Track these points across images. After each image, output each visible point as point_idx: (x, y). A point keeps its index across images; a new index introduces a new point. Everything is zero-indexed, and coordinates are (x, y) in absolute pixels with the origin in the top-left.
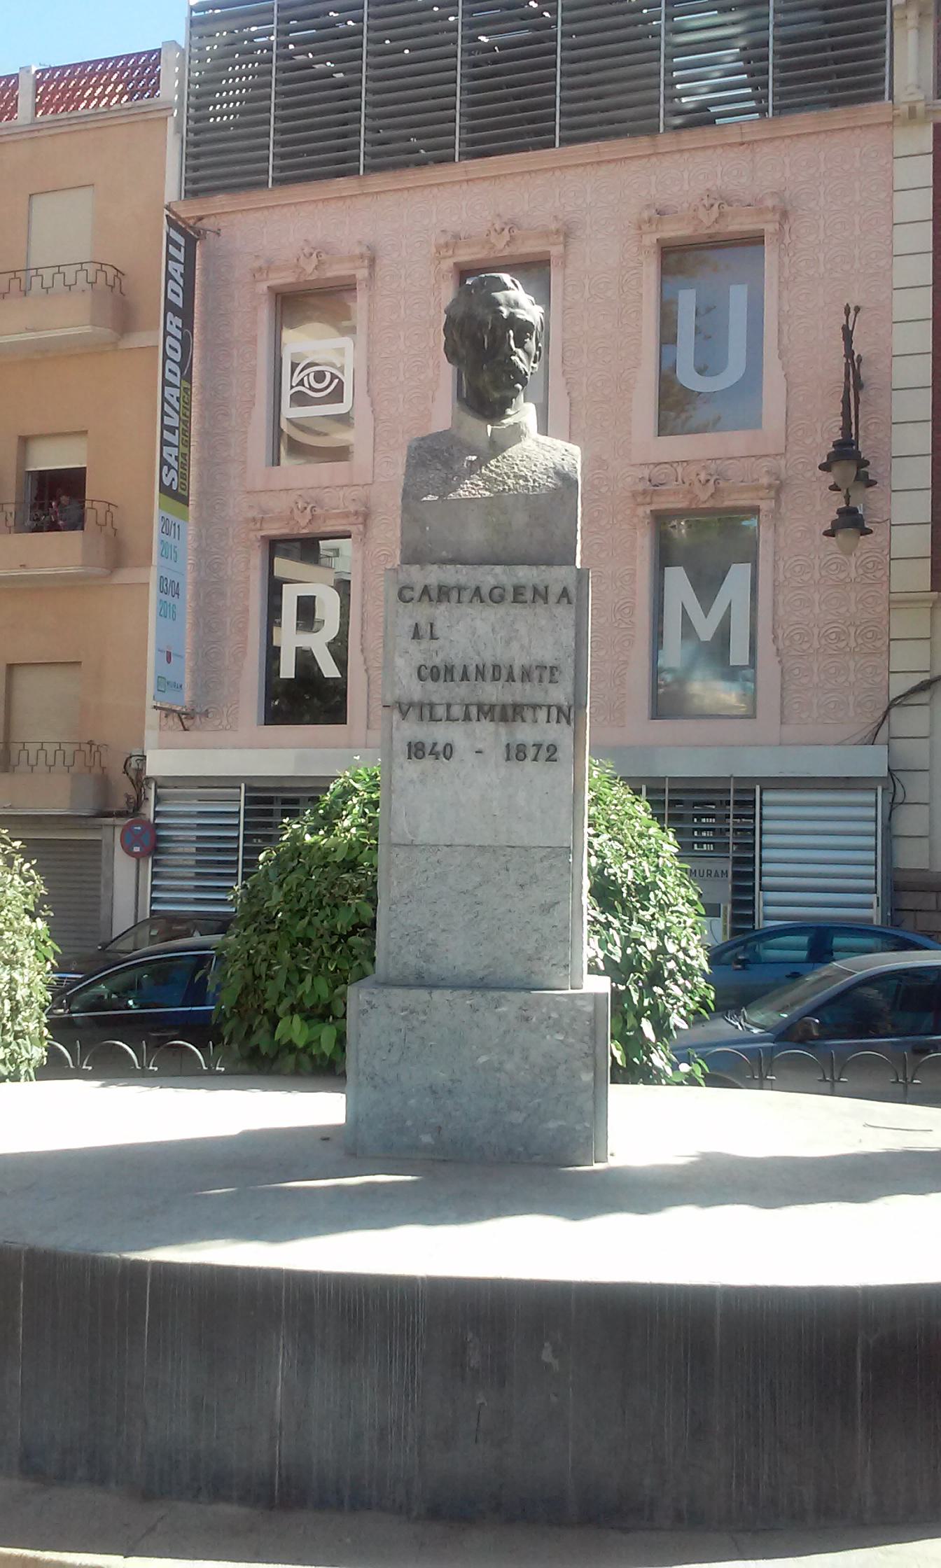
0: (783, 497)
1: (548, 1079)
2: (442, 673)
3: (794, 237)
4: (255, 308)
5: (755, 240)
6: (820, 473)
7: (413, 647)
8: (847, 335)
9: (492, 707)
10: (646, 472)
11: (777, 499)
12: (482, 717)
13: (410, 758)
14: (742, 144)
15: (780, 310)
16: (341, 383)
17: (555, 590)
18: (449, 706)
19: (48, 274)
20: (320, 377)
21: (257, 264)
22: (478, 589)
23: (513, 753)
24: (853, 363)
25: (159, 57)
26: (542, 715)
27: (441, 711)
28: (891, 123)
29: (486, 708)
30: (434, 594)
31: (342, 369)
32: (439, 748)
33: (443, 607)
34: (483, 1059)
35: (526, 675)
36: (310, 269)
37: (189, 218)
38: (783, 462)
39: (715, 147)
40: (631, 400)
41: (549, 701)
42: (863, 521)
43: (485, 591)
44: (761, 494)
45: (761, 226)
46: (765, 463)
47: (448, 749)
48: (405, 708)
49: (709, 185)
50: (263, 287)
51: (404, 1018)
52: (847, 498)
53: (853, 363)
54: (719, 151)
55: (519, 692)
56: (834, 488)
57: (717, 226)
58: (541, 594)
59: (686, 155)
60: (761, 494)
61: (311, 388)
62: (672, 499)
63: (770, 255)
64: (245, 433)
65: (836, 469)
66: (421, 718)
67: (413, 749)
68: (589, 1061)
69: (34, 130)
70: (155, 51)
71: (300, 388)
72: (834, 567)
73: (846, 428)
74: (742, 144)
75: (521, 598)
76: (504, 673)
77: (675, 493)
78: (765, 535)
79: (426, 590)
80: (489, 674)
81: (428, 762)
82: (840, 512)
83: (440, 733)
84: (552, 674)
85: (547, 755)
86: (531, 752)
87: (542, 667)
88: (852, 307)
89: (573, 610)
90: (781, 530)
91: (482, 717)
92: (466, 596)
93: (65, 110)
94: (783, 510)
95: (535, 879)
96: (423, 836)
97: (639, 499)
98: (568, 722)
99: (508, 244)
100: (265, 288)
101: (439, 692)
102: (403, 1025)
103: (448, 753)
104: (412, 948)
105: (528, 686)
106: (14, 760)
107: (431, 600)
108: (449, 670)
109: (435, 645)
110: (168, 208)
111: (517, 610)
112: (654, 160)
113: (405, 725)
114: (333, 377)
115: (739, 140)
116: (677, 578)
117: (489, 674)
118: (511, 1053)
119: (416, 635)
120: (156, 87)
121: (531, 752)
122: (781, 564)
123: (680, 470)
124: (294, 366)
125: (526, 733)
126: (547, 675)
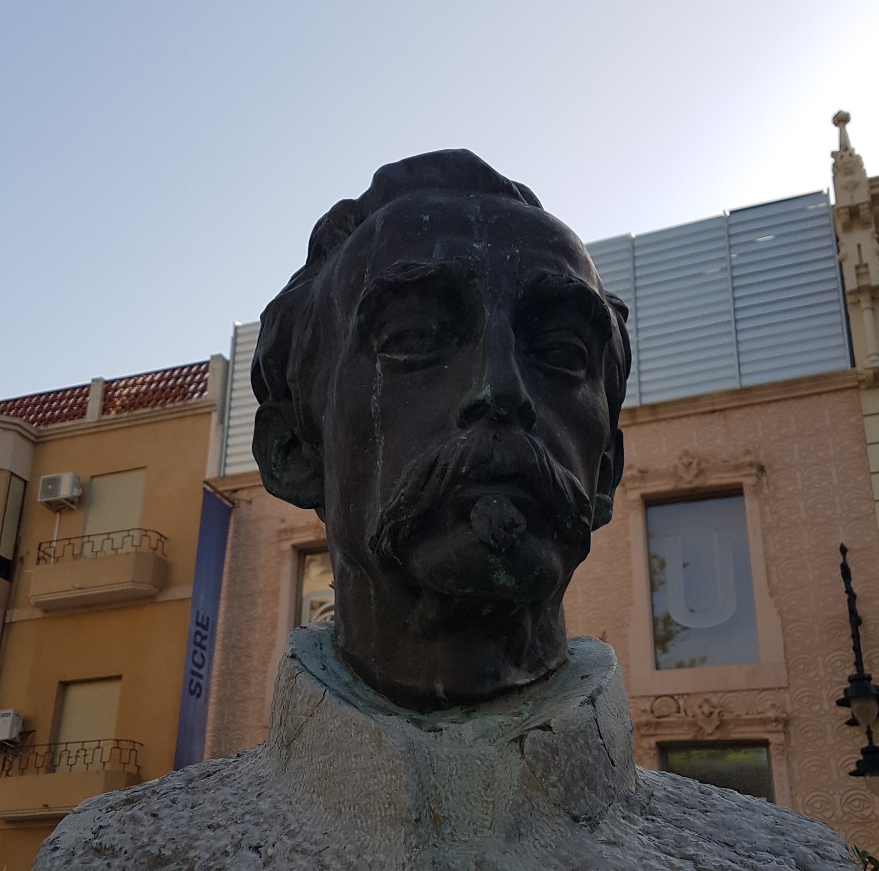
0: (791, 729)
4: (280, 563)
5: (734, 491)
10: (647, 705)
14: (714, 411)
15: (765, 553)
19: (97, 540)
21: (283, 526)
25: (207, 368)
37: (226, 491)
38: (787, 696)
44: (769, 728)
45: (739, 480)
49: (686, 447)
50: (287, 546)
52: (869, 733)
56: (853, 722)
60: (769, 728)
62: (677, 731)
63: (750, 503)
64: (265, 672)
69: (97, 430)
72: (856, 803)
73: (859, 663)
74: (714, 411)
77: (680, 725)
78: (779, 769)
82: (864, 752)
93: (173, 401)
94: (793, 743)
97: (643, 732)
115: (711, 408)
120: (84, 414)
122: (799, 799)
123: (681, 702)
124: (313, 608)
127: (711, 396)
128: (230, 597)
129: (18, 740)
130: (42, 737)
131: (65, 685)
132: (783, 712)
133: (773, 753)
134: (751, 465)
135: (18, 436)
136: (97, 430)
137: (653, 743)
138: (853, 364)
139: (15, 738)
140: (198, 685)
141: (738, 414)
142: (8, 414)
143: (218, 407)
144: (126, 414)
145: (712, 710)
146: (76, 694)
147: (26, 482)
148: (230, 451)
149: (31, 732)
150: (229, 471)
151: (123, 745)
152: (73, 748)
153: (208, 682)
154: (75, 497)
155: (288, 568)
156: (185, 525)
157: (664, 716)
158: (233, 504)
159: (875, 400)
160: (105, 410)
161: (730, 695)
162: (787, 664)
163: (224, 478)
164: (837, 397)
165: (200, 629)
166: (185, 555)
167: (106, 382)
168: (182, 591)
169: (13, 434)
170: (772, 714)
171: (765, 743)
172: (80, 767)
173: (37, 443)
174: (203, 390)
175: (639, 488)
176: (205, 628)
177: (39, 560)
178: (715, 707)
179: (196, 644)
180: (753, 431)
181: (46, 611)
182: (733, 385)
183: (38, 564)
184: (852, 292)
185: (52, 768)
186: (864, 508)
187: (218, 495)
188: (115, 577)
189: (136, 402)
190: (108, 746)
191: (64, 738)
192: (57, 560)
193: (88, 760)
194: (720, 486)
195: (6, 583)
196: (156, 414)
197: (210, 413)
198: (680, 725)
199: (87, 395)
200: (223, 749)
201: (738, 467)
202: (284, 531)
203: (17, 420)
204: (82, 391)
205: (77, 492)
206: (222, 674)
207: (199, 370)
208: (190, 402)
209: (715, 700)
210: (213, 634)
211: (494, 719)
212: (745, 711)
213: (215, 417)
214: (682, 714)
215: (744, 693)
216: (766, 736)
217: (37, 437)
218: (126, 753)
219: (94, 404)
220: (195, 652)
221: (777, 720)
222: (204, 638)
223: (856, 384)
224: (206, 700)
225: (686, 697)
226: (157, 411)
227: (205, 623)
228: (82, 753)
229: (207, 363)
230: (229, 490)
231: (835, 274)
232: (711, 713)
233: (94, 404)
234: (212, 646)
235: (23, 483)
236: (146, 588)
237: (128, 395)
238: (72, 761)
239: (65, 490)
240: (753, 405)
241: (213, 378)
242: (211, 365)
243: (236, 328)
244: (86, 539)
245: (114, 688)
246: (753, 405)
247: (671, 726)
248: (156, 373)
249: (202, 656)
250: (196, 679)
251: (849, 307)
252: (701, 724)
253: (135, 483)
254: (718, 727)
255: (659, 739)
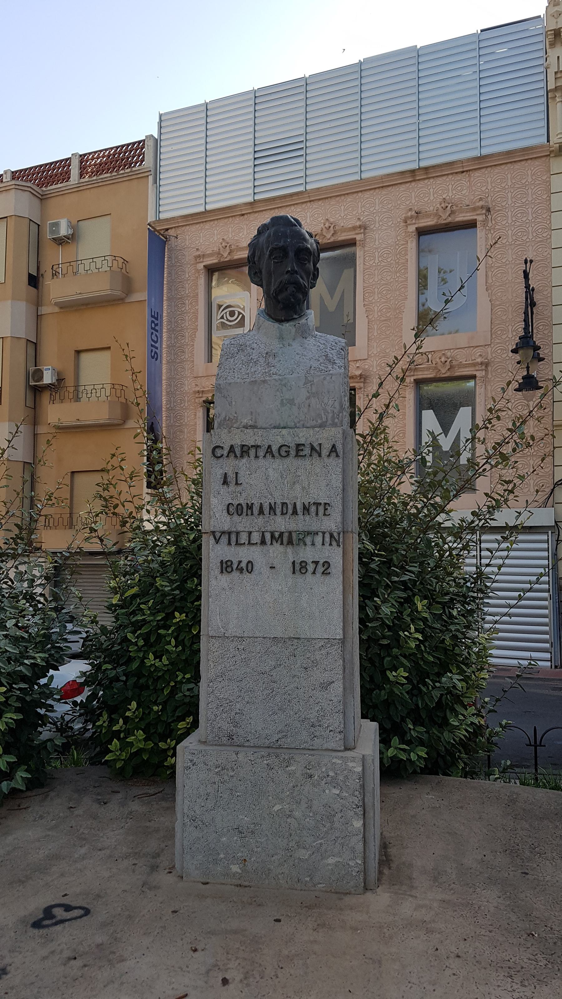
0: (489, 368)
1: (328, 825)
2: (245, 510)
3: (493, 222)
5: (471, 225)
6: (511, 354)
7: (224, 490)
8: (526, 275)
9: (281, 534)
11: (486, 371)
12: (274, 542)
13: (222, 572)
14: (463, 172)
16: (243, 317)
17: (327, 447)
18: (250, 533)
19: (87, 263)
20: (232, 314)
22: (269, 447)
23: (297, 567)
24: (529, 291)
25: (144, 144)
26: (319, 539)
27: (244, 538)
28: (549, 155)
29: (277, 535)
30: (238, 451)
31: (243, 309)
32: (243, 565)
33: (244, 460)
34: (277, 808)
35: (306, 509)
36: (225, 255)
37: (161, 230)
38: (489, 350)
39: (448, 175)
40: (402, 318)
41: (323, 529)
42: (537, 382)
43: (275, 448)
44: (477, 368)
45: (475, 217)
46: (478, 351)
47: (250, 565)
48: (218, 535)
50: (201, 266)
51: (217, 773)
52: (528, 368)
53: (529, 291)
54: (450, 177)
55: (300, 523)
57: (450, 219)
58: (315, 451)
59: (431, 180)
61: (228, 320)
63: (480, 232)
65: (521, 352)
66: (229, 543)
67: (224, 565)
68: (360, 811)
69: (78, 189)
70: (142, 141)
71: (222, 320)
73: (526, 329)
74: (463, 172)
75: (301, 453)
76: (290, 507)
77: (428, 369)
78: (480, 391)
79: (232, 449)
80: (278, 511)
81: (236, 574)
83: (243, 554)
84: (326, 509)
85: (323, 569)
86: (311, 567)
87: (317, 504)
88: (528, 259)
89: (341, 461)
90: (489, 388)
91: (274, 542)
92: (261, 453)
93: (123, 169)
94: (490, 376)
95: (315, 663)
96: (232, 630)
98: (339, 545)
99: (333, 235)
100: (202, 267)
101: (242, 524)
102: (217, 780)
103: (250, 568)
104: (224, 715)
105: (307, 518)
106: (75, 523)
107: (236, 456)
108: (250, 507)
109: (239, 488)
110: (149, 224)
111: (299, 462)
112: (413, 184)
113: (218, 547)
114: (239, 313)
116: (429, 417)
117: (278, 511)
118: (298, 803)
119: (225, 482)
121: (311, 567)
123: (430, 356)
125: (308, 554)
126: (321, 509)
127: (461, 161)
128: (169, 299)
129: (56, 384)
130: (70, 382)
131: (78, 352)
132: (486, 359)
133: (478, 382)
134: (482, 207)
135: (31, 195)
136: (78, 189)
137: (412, 380)
138: (548, 141)
139: (55, 383)
140: (156, 353)
141: (477, 174)
142: (34, 183)
143: (152, 173)
144: (95, 178)
145: (447, 359)
146: (84, 357)
147: (39, 225)
148: (161, 202)
149: (63, 380)
150: (163, 216)
151: (116, 387)
152: (89, 388)
153: (161, 351)
154: (70, 234)
155: (202, 281)
156: (139, 253)
157: (420, 365)
158: (166, 238)
159: (559, 164)
160: (81, 175)
161: (458, 350)
162: (491, 331)
163: (159, 221)
164: (537, 162)
165: (153, 319)
166: (140, 269)
167: (81, 156)
168: (141, 295)
169: (28, 193)
170: (479, 360)
171: (474, 377)
172: (94, 398)
173: (43, 199)
174: (142, 161)
175: (415, 224)
176: (157, 319)
177: (53, 276)
178: (448, 358)
179: (152, 328)
180: (484, 185)
181: (61, 308)
182: (476, 153)
183: (53, 278)
184: (551, 90)
185: (77, 399)
186: (544, 235)
187: (156, 233)
188: (101, 287)
189: (100, 169)
190: (108, 387)
191: (82, 382)
192: (64, 275)
193: (98, 395)
194: (463, 222)
195: (35, 290)
196: (114, 178)
197: (148, 176)
198: (428, 369)
199: (69, 165)
200: (172, 390)
201: (474, 209)
202: (199, 256)
203: (29, 184)
204: (67, 162)
205: (71, 232)
206: (168, 347)
207: (139, 145)
208: (134, 169)
209: (449, 354)
210: (161, 322)
211: (292, 323)
212: (465, 360)
213: (151, 178)
214: (430, 363)
215: (466, 349)
216: (475, 373)
217: (42, 195)
218: (118, 392)
219: (75, 171)
220: (152, 333)
221: (482, 363)
222: (156, 325)
223: (549, 153)
224: (161, 362)
225: (433, 353)
226: (114, 176)
227: (156, 316)
228: (94, 391)
229: (144, 141)
230: (163, 229)
231: (542, 77)
232: (446, 362)
233: (75, 171)
234: (161, 330)
235: (37, 226)
236: (118, 293)
237: (95, 165)
238: (89, 395)
239: (64, 231)
240: (487, 167)
241: (148, 152)
242: (146, 142)
243: (161, 116)
244: (80, 262)
245: (106, 355)
246: (487, 167)
247: (423, 370)
248: (112, 148)
249: (156, 336)
250: (154, 349)
251: (549, 101)
252: (440, 368)
253: (104, 225)
254: (449, 369)
255: (415, 377)
